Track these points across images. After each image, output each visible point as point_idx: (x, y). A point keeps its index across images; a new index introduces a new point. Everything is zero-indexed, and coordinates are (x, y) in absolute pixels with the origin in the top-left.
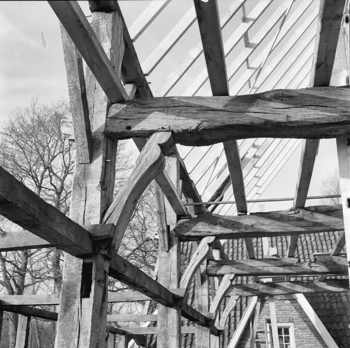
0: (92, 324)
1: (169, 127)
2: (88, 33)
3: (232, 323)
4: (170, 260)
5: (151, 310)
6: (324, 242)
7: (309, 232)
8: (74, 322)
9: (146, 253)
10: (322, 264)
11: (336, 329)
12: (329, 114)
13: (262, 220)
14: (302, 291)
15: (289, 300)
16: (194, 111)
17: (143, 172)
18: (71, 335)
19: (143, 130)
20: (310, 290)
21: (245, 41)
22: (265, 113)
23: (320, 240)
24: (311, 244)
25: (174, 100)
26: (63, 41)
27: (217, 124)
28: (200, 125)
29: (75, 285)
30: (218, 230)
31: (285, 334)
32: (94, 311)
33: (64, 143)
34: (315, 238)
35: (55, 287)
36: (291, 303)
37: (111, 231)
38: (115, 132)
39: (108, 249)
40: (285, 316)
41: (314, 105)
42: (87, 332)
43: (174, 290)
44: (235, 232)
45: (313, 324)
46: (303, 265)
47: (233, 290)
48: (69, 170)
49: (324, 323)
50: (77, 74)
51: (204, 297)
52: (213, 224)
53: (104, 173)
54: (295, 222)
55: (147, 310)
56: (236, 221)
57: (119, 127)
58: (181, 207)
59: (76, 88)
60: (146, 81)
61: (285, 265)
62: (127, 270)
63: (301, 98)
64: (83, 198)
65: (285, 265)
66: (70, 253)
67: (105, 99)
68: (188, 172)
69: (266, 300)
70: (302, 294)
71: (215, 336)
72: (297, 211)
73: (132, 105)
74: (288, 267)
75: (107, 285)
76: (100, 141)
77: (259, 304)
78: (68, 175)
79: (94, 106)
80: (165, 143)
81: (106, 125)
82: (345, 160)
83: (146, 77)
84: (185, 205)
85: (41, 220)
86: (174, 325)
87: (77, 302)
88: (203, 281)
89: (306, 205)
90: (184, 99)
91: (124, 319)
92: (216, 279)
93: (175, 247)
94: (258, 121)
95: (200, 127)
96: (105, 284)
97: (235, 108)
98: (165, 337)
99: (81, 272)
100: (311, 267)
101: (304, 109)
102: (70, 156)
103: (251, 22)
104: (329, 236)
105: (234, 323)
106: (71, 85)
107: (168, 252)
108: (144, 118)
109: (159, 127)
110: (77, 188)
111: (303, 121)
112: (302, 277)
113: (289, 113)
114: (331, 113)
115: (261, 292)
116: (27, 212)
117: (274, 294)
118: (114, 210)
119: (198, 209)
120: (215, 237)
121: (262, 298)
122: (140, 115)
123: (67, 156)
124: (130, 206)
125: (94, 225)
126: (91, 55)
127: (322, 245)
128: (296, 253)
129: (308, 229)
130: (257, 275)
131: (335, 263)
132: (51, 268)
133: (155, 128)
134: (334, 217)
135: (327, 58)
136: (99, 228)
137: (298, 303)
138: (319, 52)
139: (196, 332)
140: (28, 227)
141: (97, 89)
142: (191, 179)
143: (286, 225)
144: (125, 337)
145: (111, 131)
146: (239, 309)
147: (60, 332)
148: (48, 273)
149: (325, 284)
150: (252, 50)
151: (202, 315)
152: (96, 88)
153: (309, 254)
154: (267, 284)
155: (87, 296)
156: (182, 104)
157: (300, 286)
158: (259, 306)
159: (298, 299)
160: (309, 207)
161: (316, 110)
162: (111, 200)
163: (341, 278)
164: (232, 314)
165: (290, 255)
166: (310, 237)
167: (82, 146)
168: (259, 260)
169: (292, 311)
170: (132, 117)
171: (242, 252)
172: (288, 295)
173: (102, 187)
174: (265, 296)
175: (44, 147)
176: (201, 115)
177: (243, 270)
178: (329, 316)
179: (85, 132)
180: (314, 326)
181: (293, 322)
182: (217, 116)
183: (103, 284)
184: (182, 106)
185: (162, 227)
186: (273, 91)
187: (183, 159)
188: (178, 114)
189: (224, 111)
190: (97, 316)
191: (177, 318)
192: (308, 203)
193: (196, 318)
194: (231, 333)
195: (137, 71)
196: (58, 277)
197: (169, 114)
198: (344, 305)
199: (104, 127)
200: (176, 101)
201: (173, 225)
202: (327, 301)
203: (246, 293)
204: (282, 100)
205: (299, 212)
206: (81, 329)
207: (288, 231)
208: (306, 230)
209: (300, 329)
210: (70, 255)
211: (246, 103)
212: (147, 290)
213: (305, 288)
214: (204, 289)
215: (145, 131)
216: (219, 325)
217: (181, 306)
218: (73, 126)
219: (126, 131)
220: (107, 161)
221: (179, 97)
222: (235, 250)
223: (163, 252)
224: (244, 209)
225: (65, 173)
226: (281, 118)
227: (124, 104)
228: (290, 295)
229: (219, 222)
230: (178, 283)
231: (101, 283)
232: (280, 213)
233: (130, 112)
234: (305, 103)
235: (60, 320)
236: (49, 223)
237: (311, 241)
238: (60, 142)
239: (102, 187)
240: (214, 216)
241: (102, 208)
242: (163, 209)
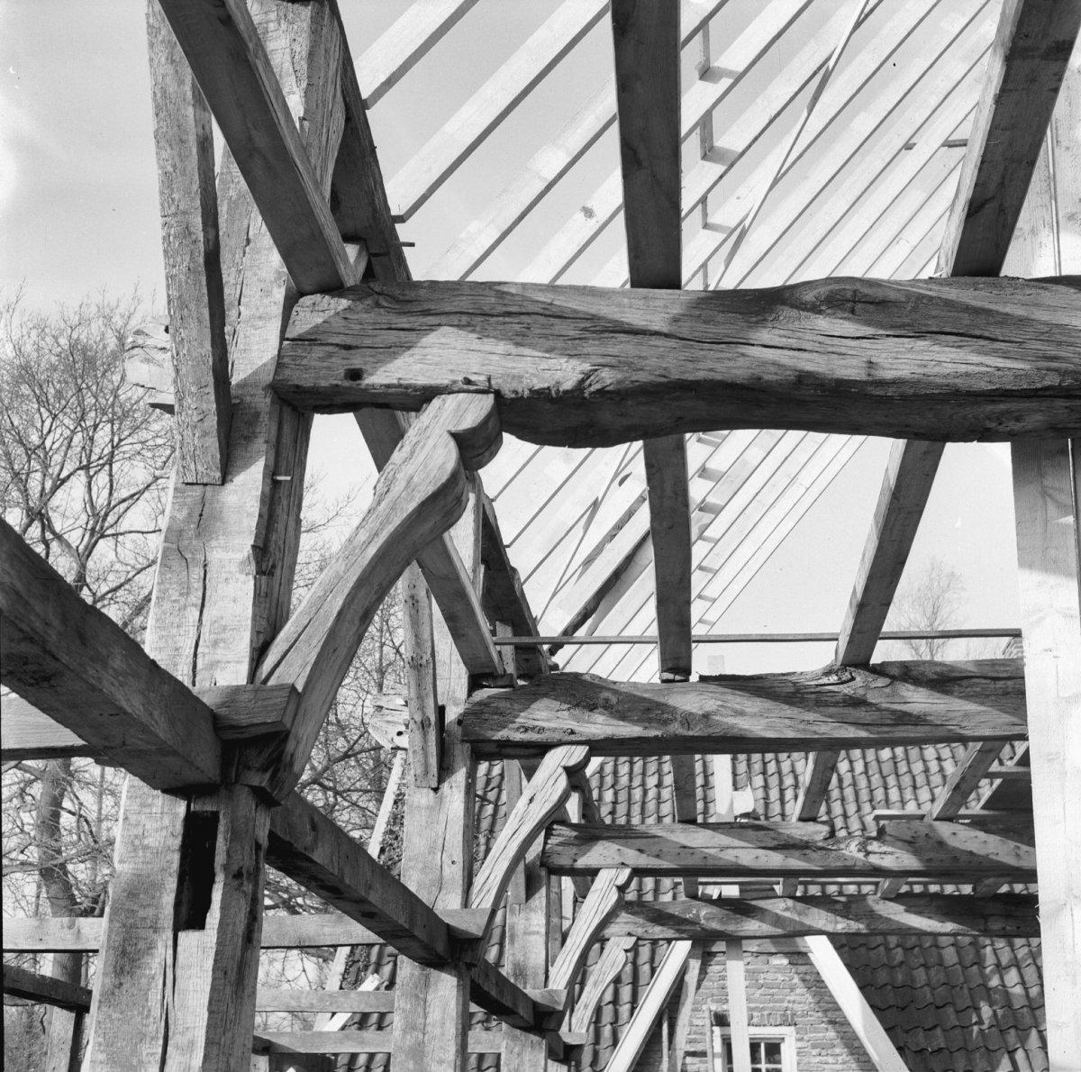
0: (209, 1018)
1: (489, 380)
2: (247, 47)
3: (607, 1025)
4: (442, 818)
5: (351, 978)
6: (891, 781)
7: (879, 744)
8: (149, 1011)
9: (337, 793)
10: (900, 844)
11: (922, 1050)
12: (1001, 363)
13: (753, 705)
14: (830, 928)
15: (786, 954)
16: (572, 333)
17: (397, 521)
18: (134, 1052)
19: (400, 386)
20: (855, 926)
21: (703, 141)
22: (799, 350)
23: (881, 772)
24: (854, 784)
25: (507, 293)
26: (154, 75)
27: (643, 377)
28: (588, 378)
29: (157, 887)
30: (600, 726)
31: (769, 1061)
32: (220, 974)
33: (92, 439)
34: (866, 765)
35: (38, 897)
36: (790, 963)
37: (285, 708)
38: (308, 388)
39: (271, 770)
40: (771, 1005)
41: (954, 331)
42: (192, 1043)
43: (452, 913)
44: (652, 733)
45: (854, 1032)
46: (842, 846)
47: (618, 920)
48: (106, 524)
49: (887, 1030)
50: (196, 186)
51: (533, 938)
52: (584, 707)
53: (266, 517)
54: (841, 710)
55: (340, 977)
56: (656, 699)
57: (323, 371)
58: (487, 648)
59: (187, 231)
60: (397, 238)
61: (787, 846)
62: (320, 845)
63: (915, 309)
64: (195, 598)
65: (787, 846)
66: (143, 779)
67: (280, 279)
68: (506, 542)
69: (714, 954)
70: (824, 938)
71: (556, 1064)
72: (846, 676)
73: (369, 301)
74: (797, 853)
75: (260, 887)
76: (257, 414)
77: (695, 965)
78: (101, 541)
79: (242, 300)
80: (473, 432)
81: (280, 364)
82: (1036, 511)
83: (398, 227)
84: (496, 644)
85: (65, 659)
86: (448, 1024)
87: (160, 944)
88: (530, 890)
89: (876, 659)
90: (540, 290)
91: (276, 1003)
92: (567, 883)
93: (460, 777)
94: (776, 374)
95: (590, 385)
96: (256, 884)
97: (701, 329)
98: (416, 1063)
99: (178, 842)
100: (868, 853)
101: (921, 344)
102: (111, 481)
103: (726, 82)
104: (908, 763)
105: (611, 1024)
106: (172, 221)
107: (436, 790)
108: (408, 347)
109: (457, 378)
110: (176, 564)
111: (918, 381)
112: (823, 885)
113: (872, 353)
114: (1007, 361)
115: (703, 929)
116: (24, 626)
117: (742, 934)
118: (296, 641)
119: (527, 660)
120: (588, 748)
121: (705, 945)
122: (392, 337)
123: (102, 479)
124: (348, 631)
125: (228, 687)
126: (250, 125)
127: (886, 788)
128: (823, 809)
129: (878, 733)
130: (694, 872)
131: (941, 844)
132: (32, 834)
133: (442, 379)
134: (960, 698)
135: (1006, 183)
136: (245, 697)
137: (812, 964)
138: (982, 162)
139: (503, 1050)
140: (19, 679)
141: (252, 245)
142: (513, 564)
143: (810, 716)
144: (270, 1060)
145: (296, 382)
146: (633, 980)
147: (100, 1044)
148: (22, 852)
149: (902, 908)
150: (720, 169)
151: (525, 995)
152: (248, 241)
153: (845, 816)
154: (722, 902)
155: (197, 922)
156: (531, 308)
157: (823, 913)
158: (697, 971)
159: (811, 952)
160: (883, 664)
161: (960, 347)
162: (285, 609)
163: (942, 889)
164: (608, 997)
165: (804, 816)
166: (851, 762)
167: (199, 424)
168: (708, 828)
169: (792, 990)
170: (368, 342)
171: (644, 803)
172: (783, 940)
173: (257, 563)
174: (714, 942)
175: (30, 452)
176: (592, 347)
177: (658, 856)
178: (903, 1009)
179: (210, 379)
180: (857, 1038)
181: (796, 1025)
182: (645, 351)
183: (246, 880)
184: (533, 313)
185: (422, 708)
186: (829, 280)
187: (493, 500)
188: (520, 339)
189: (666, 335)
190: (228, 990)
191: (457, 1004)
192: (883, 652)
193: (509, 1004)
194: (603, 1055)
195: (372, 203)
196: (55, 862)
197: (488, 336)
198: (947, 976)
199: (273, 368)
200: (513, 295)
201: (456, 704)
202: (896, 962)
203: (657, 931)
204: (853, 311)
205: (853, 679)
206: (170, 1034)
207: (816, 736)
208: (872, 736)
209: (814, 1047)
210: (142, 783)
211: (739, 316)
212: (373, 910)
213: (839, 918)
214: (533, 915)
215: (407, 387)
216: (570, 1030)
217: (470, 966)
218: (173, 357)
219: (347, 384)
220: (279, 478)
221: (524, 285)
222: (623, 796)
223: (421, 790)
224: (682, 664)
225: (92, 535)
226: (849, 368)
227: (341, 296)
228: (789, 941)
229: (601, 702)
230: (463, 892)
231: (245, 883)
232: (793, 678)
233: (361, 324)
234: (926, 325)
235: (100, 1001)
236: (91, 672)
237: (853, 777)
238: (80, 434)
239: (258, 563)
240: (585, 681)
241: (258, 632)
242: (429, 652)
